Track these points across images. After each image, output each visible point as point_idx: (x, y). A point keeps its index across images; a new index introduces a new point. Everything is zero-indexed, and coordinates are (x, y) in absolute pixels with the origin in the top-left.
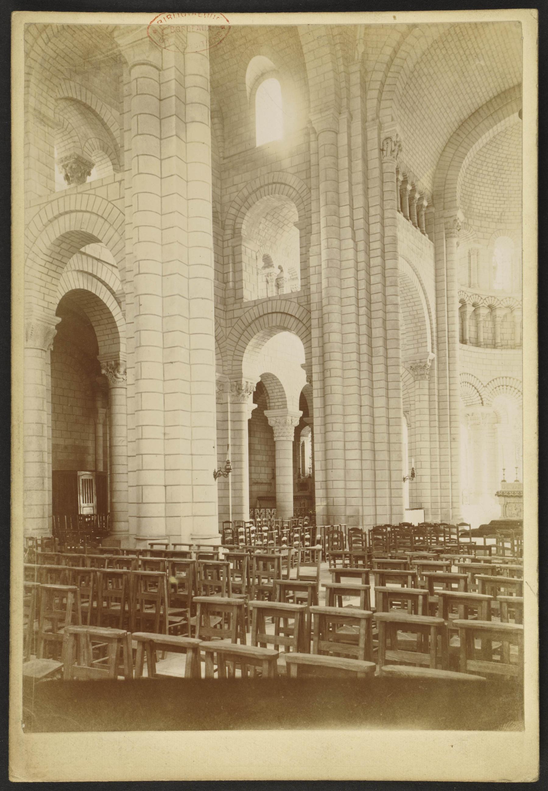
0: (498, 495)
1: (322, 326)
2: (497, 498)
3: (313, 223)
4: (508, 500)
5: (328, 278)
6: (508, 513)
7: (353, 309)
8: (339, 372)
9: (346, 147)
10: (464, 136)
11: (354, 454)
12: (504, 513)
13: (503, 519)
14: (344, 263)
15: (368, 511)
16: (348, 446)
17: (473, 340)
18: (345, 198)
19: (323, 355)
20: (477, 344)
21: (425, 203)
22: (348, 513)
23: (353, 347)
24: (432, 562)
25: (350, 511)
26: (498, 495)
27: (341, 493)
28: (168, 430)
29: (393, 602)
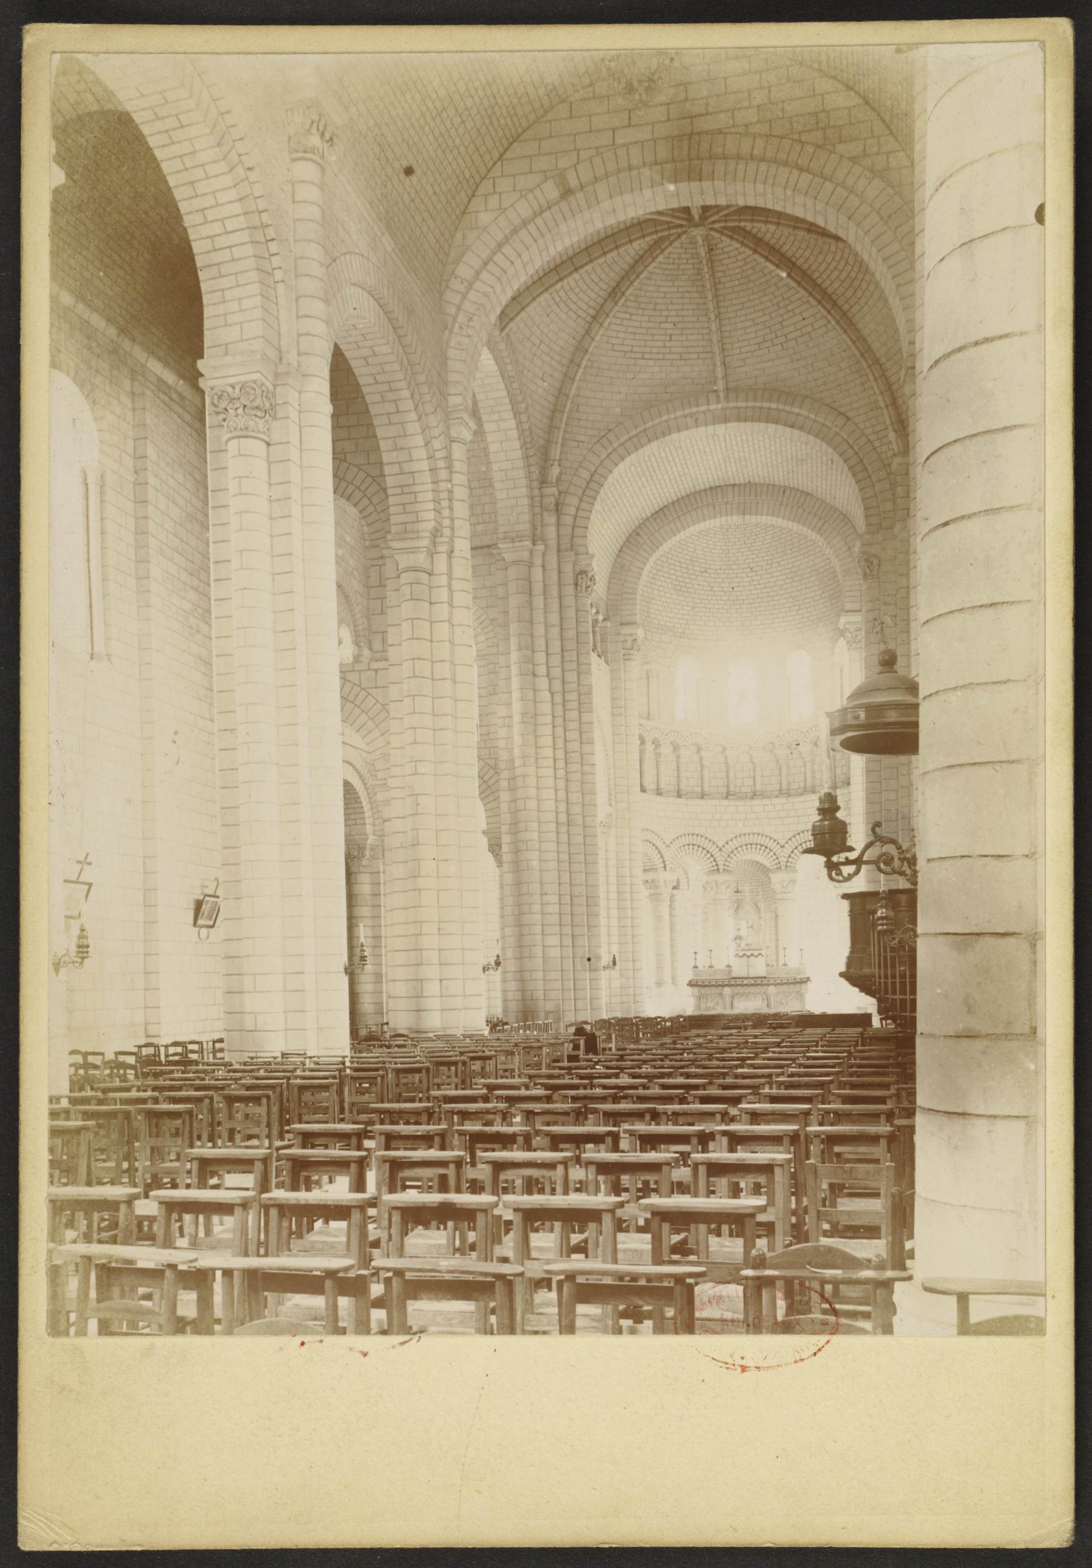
0: (691, 984)
1: (512, 789)
2: (690, 988)
3: (143, 361)
4: (703, 990)
5: (523, 735)
6: (703, 1006)
7: (551, 772)
8: (536, 845)
9: (541, 584)
10: (646, 538)
11: (554, 940)
12: (698, 1007)
13: (697, 1013)
14: (539, 718)
15: (569, 1005)
16: (547, 930)
17: (654, 787)
18: (540, 643)
19: (515, 823)
20: (659, 793)
21: (601, 618)
22: (547, 1009)
23: (551, 816)
24: (523, 1092)
25: (549, 1006)
26: (691, 984)
27: (540, 985)
28: (442, 926)
29: (408, 1183)
